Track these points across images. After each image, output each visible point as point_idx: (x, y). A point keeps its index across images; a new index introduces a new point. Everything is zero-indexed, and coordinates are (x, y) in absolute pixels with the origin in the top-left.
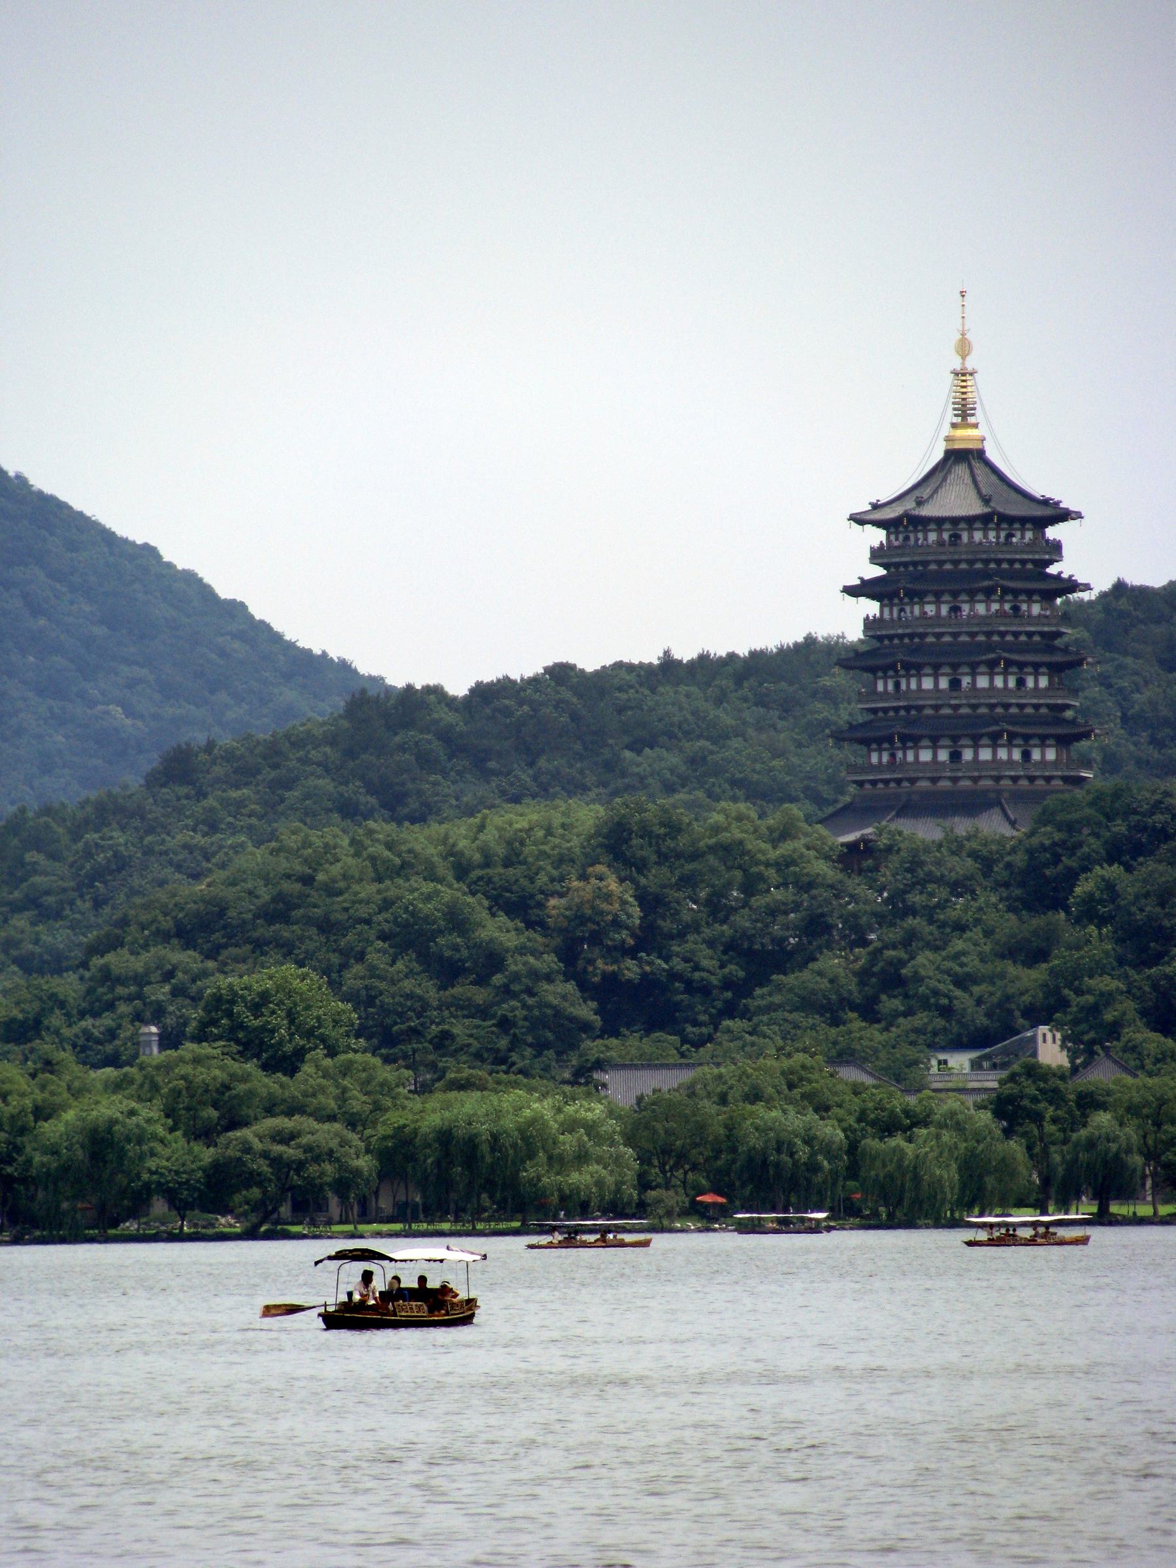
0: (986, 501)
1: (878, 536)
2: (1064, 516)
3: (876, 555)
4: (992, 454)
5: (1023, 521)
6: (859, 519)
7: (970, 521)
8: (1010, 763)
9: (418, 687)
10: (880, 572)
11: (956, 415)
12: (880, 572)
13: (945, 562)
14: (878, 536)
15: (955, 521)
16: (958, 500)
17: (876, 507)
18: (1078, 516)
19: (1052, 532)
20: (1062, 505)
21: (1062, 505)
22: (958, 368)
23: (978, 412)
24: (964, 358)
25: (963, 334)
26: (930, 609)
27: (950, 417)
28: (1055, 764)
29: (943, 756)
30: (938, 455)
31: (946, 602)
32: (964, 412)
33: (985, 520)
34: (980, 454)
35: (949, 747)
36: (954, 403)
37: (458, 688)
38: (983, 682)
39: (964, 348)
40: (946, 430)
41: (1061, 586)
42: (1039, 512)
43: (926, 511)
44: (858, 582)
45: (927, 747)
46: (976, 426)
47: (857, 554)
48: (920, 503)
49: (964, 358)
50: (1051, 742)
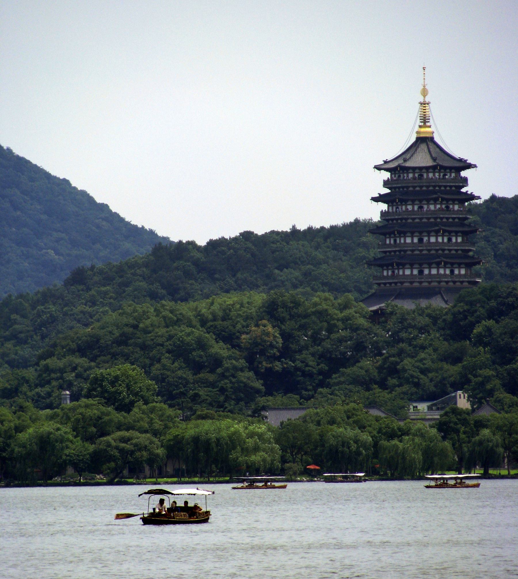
0: (434, 159)
1: (387, 175)
2: (469, 166)
3: (386, 184)
4: (437, 139)
5: (451, 168)
6: (378, 168)
7: (427, 168)
8: (445, 275)
9: (184, 242)
10: (387, 191)
11: (421, 122)
12: (387, 191)
14: (387, 175)
15: (421, 168)
16: (422, 159)
17: (386, 162)
18: (475, 166)
19: (463, 174)
20: (468, 162)
21: (468, 162)
22: (422, 101)
23: (431, 120)
24: (424, 96)
26: (410, 208)
27: (419, 123)
28: (465, 276)
29: (415, 272)
30: (413, 140)
31: (417, 204)
32: (425, 120)
33: (434, 168)
34: (432, 139)
35: (418, 268)
36: (420, 117)
37: (202, 242)
38: (433, 240)
39: (424, 92)
40: (417, 129)
42: (457, 164)
43: (408, 164)
44: (378, 195)
45: (408, 268)
46: (430, 127)
47: (377, 183)
48: (405, 161)
49: (424, 96)
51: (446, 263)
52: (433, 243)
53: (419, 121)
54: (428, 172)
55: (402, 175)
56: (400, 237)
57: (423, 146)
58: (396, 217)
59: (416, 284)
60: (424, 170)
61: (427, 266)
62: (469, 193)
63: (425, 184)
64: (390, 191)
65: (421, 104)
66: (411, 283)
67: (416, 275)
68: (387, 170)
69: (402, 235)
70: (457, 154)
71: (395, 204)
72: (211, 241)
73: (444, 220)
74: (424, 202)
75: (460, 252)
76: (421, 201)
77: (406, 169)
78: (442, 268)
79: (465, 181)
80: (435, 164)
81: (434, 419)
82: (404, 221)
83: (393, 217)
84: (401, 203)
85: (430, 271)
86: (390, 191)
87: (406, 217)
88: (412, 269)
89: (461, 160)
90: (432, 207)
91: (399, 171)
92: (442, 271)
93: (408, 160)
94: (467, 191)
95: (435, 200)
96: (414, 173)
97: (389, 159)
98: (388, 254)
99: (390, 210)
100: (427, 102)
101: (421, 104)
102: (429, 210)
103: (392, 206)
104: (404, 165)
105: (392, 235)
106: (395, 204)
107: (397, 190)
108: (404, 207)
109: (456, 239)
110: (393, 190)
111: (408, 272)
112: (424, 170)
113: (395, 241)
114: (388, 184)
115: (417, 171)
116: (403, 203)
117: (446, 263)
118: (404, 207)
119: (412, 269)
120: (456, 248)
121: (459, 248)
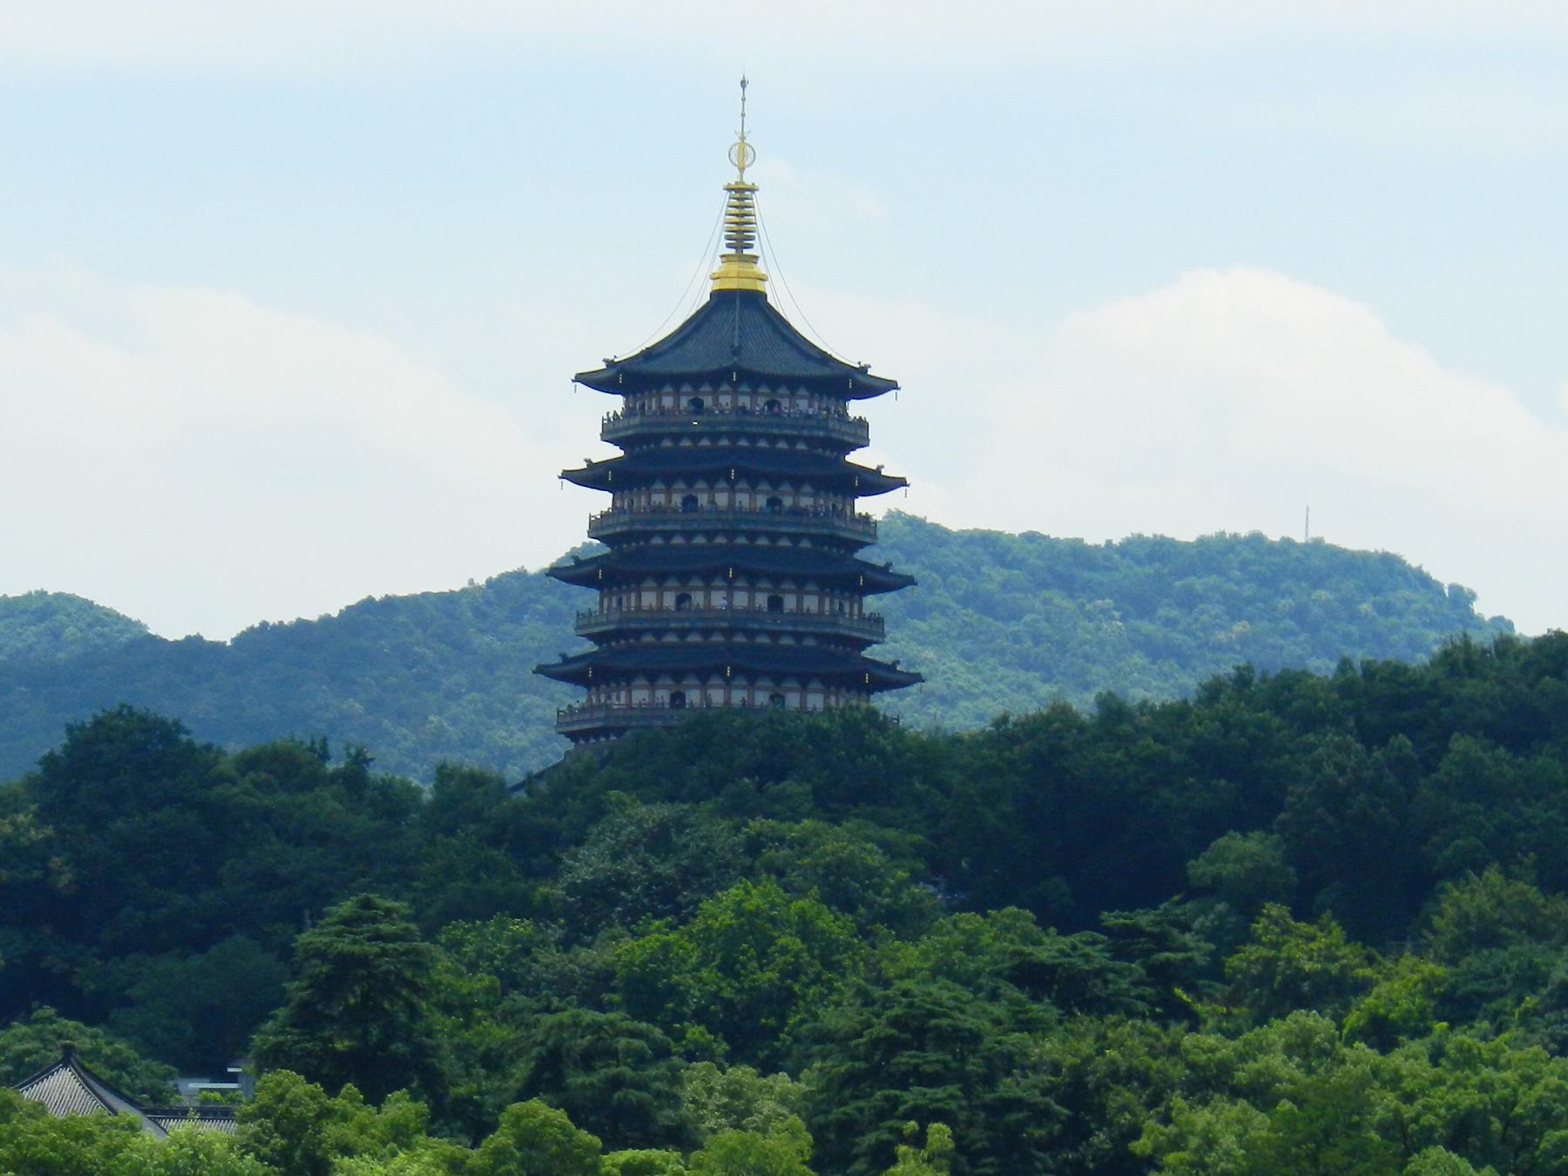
2: (870, 387)
3: (611, 432)
6: (590, 380)
8: (751, 612)
9: (335, 614)
10: (615, 452)
11: (729, 246)
12: (615, 452)
13: (716, 533)
15: (774, 381)
18: (892, 385)
19: (855, 408)
20: (870, 372)
21: (870, 372)
24: (742, 170)
25: (743, 138)
26: (668, 402)
31: (687, 394)
32: (740, 239)
35: (677, 589)
36: (728, 238)
39: (742, 154)
41: (895, 677)
44: (584, 465)
45: (651, 589)
47: (585, 427)
49: (742, 170)
50: (811, 587)
61: (700, 584)
64: (620, 453)
70: (846, 351)
75: (809, 642)
79: (859, 434)
85: (800, 602)
86: (620, 453)
89: (863, 370)
90: (722, 499)
100: (748, 182)
103: (622, 499)
120: (792, 530)
121: (802, 530)
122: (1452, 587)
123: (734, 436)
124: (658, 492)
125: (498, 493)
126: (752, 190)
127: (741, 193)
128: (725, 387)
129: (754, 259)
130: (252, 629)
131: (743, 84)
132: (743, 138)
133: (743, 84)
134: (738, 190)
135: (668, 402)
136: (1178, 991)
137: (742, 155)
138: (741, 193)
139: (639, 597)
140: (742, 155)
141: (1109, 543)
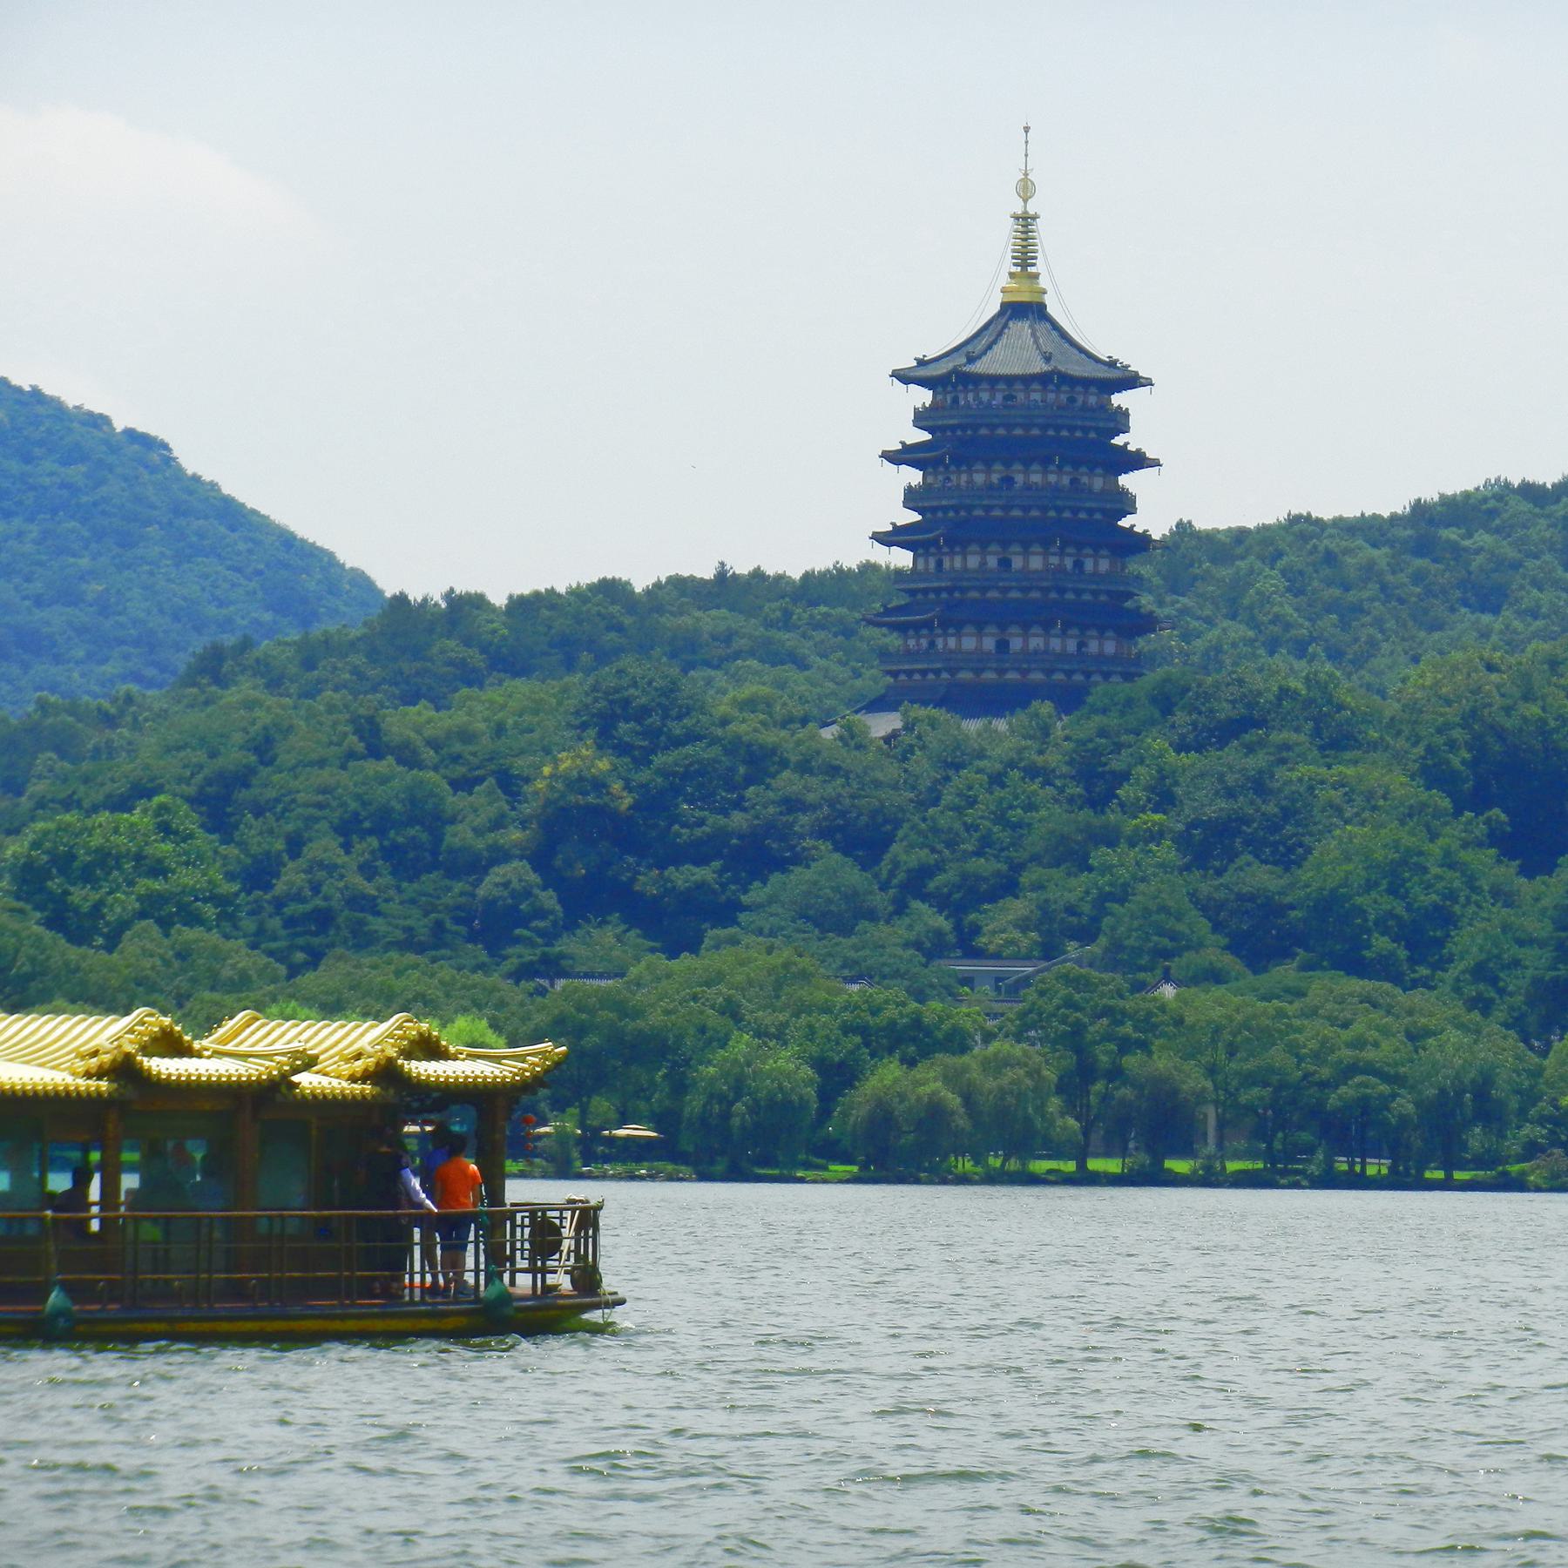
1: (924, 397)
2: (1132, 381)
4: (1053, 310)
5: (1087, 383)
6: (903, 377)
7: (1027, 380)
14: (924, 397)
15: (1010, 380)
16: (1016, 355)
17: (921, 363)
18: (1155, 463)
19: (1118, 399)
24: (1025, 201)
25: (1026, 174)
32: (1025, 258)
33: (1043, 379)
37: (1386, 515)
39: (1026, 189)
40: (1004, 281)
43: (979, 367)
45: (971, 635)
47: (899, 415)
48: (971, 359)
49: (1025, 201)
50: (1104, 552)
51: (1067, 626)
52: (1036, 571)
53: (1009, 261)
54: (1027, 390)
55: (961, 396)
56: (952, 553)
57: (1021, 329)
58: (944, 503)
59: (989, 676)
60: (1018, 386)
62: (1131, 448)
63: (1020, 420)
64: (919, 518)
65: (1017, 218)
66: (984, 590)
67: (989, 653)
68: (922, 382)
69: (951, 631)
70: (1102, 349)
71: (941, 469)
72: (628, 583)
73: (1067, 514)
74: (1016, 548)
75: (1103, 598)
76: (1005, 544)
77: (975, 380)
78: (1056, 636)
80: (1046, 368)
81: (1033, 334)
82: (957, 595)
83: (935, 503)
84: (965, 387)
85: (1026, 561)
86: (919, 518)
87: (968, 502)
88: (980, 634)
89: (1112, 364)
90: (1036, 478)
91: (947, 467)
92: (1056, 644)
93: (979, 357)
94: (1127, 444)
95: (1046, 461)
96: (993, 390)
97: (931, 354)
98: (919, 596)
99: (921, 566)
100: (1031, 212)
101: (1017, 218)
102: (1028, 487)
104: (967, 369)
105: (933, 550)
106: (941, 469)
107: (940, 514)
108: (970, 396)
109: (1096, 564)
110: (929, 515)
111: (969, 643)
112: (1018, 386)
113: (939, 564)
114: (926, 419)
115: (1001, 386)
116: (957, 549)
117: (1067, 626)
118: (964, 477)
119: (980, 634)
122: (448, 595)
123: (1044, 427)
124: (1036, 472)
125: (828, 498)
126: (1034, 218)
127: (1025, 221)
128: (1051, 387)
129: (1036, 276)
130: (611, 590)
131: (1027, 129)
132: (1026, 174)
133: (1027, 129)
134: (1025, 219)
135: (985, 396)
136: (417, 1231)
137: (1025, 188)
138: (1025, 221)
139: (965, 559)
140: (1025, 188)
141: (1309, 514)
